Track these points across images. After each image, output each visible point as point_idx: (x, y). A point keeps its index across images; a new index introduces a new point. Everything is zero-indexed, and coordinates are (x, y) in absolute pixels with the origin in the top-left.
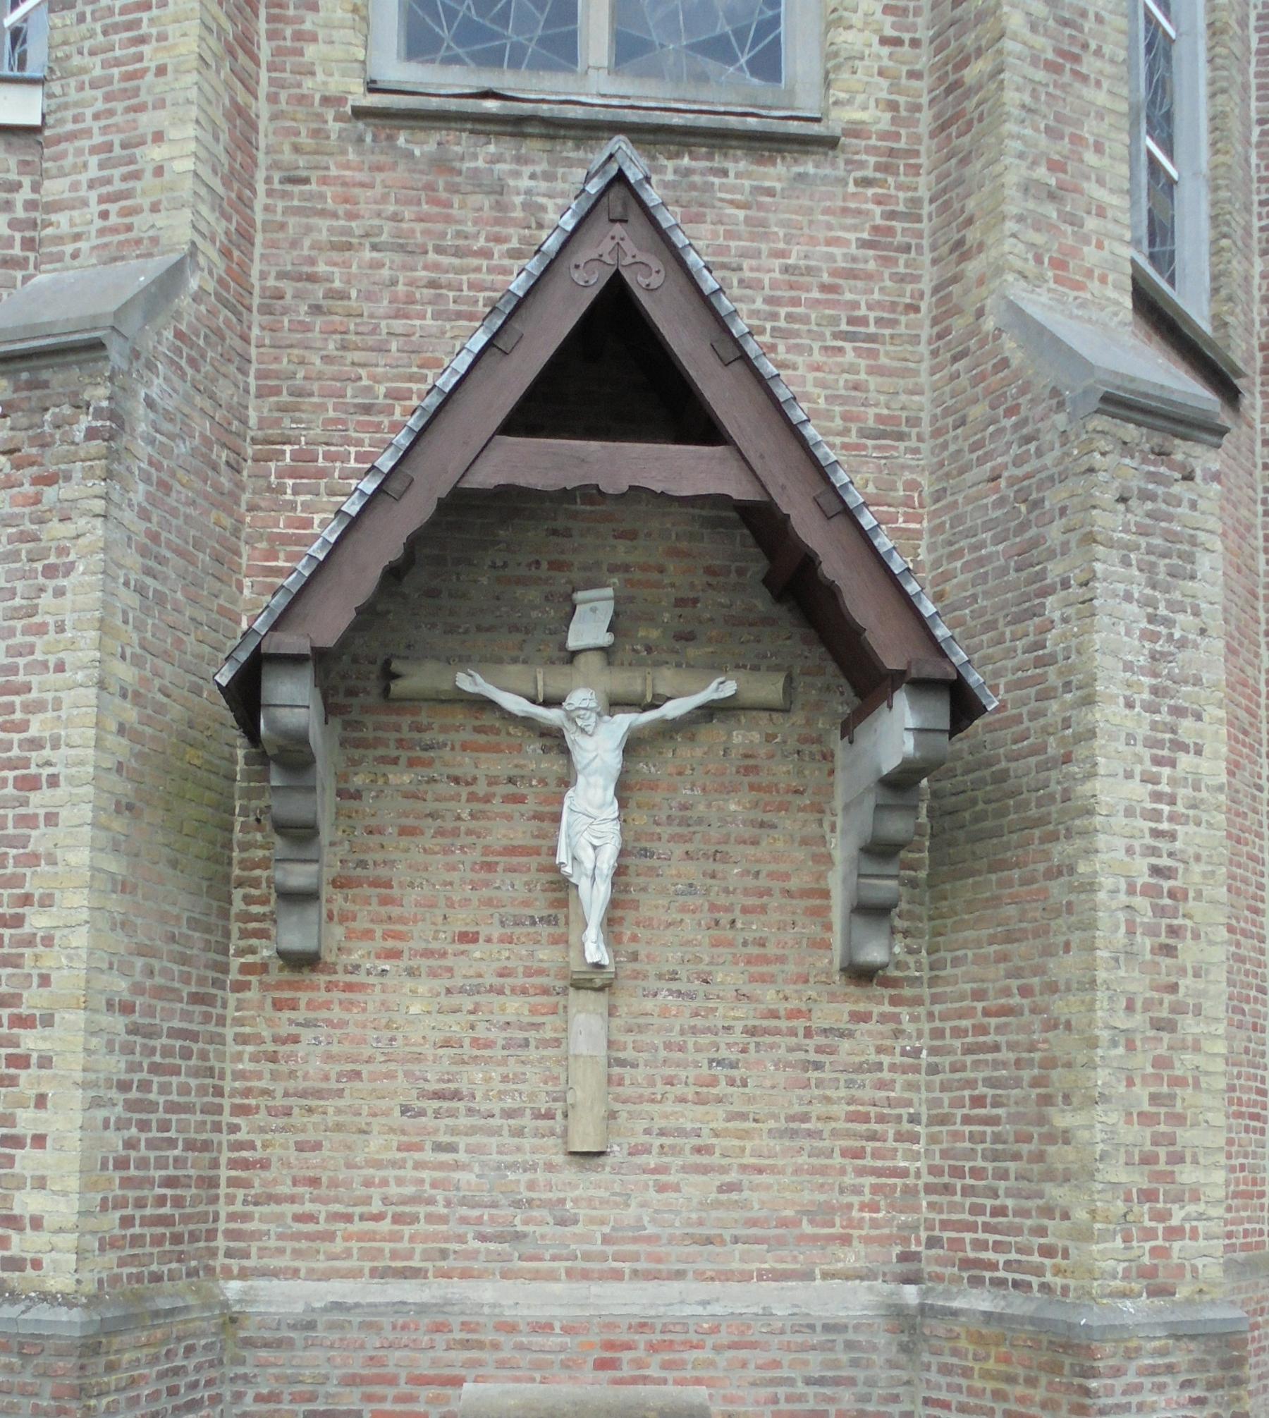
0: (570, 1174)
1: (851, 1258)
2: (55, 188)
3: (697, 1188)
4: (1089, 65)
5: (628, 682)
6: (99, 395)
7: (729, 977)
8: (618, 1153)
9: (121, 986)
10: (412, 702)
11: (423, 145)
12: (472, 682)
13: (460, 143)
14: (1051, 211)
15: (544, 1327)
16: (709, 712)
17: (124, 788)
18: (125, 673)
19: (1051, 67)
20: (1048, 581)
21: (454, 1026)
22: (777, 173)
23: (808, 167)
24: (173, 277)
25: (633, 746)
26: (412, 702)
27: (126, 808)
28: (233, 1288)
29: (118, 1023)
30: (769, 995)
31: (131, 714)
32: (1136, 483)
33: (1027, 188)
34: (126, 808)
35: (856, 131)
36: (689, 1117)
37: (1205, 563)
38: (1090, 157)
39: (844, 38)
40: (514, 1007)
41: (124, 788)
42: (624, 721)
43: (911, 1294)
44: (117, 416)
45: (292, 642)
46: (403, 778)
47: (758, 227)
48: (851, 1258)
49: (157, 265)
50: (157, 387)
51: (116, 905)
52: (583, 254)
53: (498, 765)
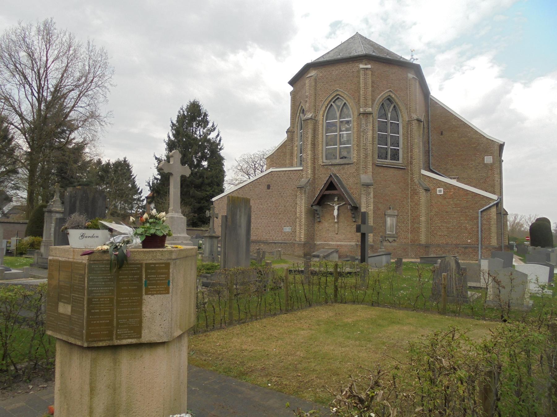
0: (336, 235)
1: (354, 241)
2: (303, 173)
3: (344, 236)
4: (368, 157)
5: (339, 202)
6: (304, 189)
7: (346, 222)
8: (339, 233)
9: (307, 224)
10: (325, 205)
11: (326, 167)
12: (329, 203)
13: (328, 166)
14: (365, 169)
15: (334, 245)
16: (344, 204)
17: (307, 212)
18: (306, 205)
19: (365, 158)
20: (337, 206)
21: (329, 225)
22: (349, 166)
23: (351, 165)
24: (309, 180)
25: (339, 207)
26: (325, 205)
27: (306, 213)
28: (315, 242)
29: (307, 226)
30: (348, 223)
31: (307, 208)
32: (365, 189)
33: (363, 167)
34: (306, 213)
35: (354, 162)
36: (343, 231)
37: (371, 194)
38: (368, 164)
39: (354, 155)
40: (332, 224)
41: (307, 212)
42: (337, 206)
43: (358, 243)
44: (305, 191)
45: (314, 204)
46: (325, 209)
47: (348, 170)
48: (354, 241)
49: (309, 179)
50: (308, 188)
51: (306, 219)
52: (329, 179)
53: (331, 208)
